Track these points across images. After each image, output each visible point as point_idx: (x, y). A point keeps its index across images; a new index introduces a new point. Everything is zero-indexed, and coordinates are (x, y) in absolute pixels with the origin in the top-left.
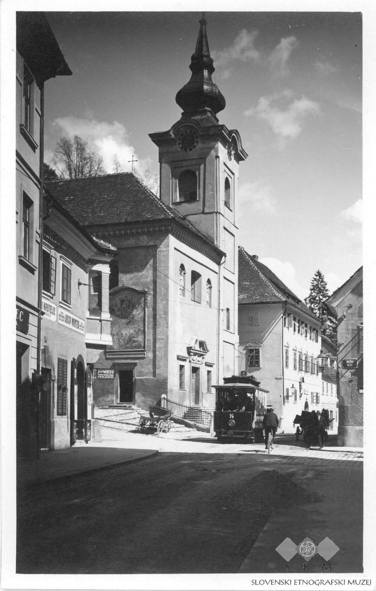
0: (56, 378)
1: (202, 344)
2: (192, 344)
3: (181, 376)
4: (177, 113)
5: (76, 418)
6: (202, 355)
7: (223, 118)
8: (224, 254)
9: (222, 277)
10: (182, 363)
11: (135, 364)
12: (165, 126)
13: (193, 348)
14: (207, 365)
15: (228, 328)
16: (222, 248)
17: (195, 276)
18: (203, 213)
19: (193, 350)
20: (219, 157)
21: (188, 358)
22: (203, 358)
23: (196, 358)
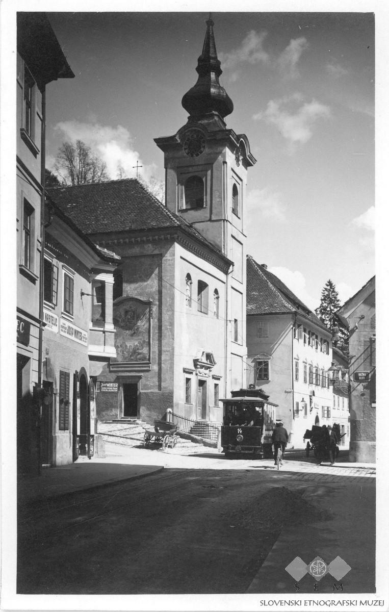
0: (58, 392)
1: (209, 356)
2: (199, 357)
3: (188, 389)
4: (183, 117)
5: (79, 433)
6: (209, 368)
7: (231, 122)
9: (229, 287)
10: (188, 376)
11: (140, 377)
12: (171, 130)
13: (200, 361)
15: (236, 339)
17: (202, 286)
18: (210, 220)
20: (226, 163)
21: (194, 371)
23: (203, 370)
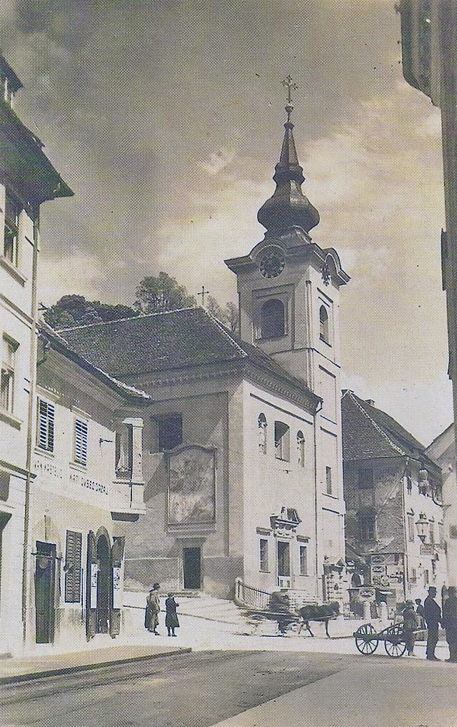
0: (64, 556)
1: (292, 513)
2: (278, 513)
3: (263, 554)
4: (260, 232)
5: (94, 606)
6: (293, 527)
7: (318, 235)
9: (318, 429)
10: (264, 537)
11: (203, 540)
12: (243, 248)
13: (279, 518)
15: (329, 491)
17: (281, 429)
18: (292, 349)
20: (310, 282)
21: (271, 531)
23: (284, 531)
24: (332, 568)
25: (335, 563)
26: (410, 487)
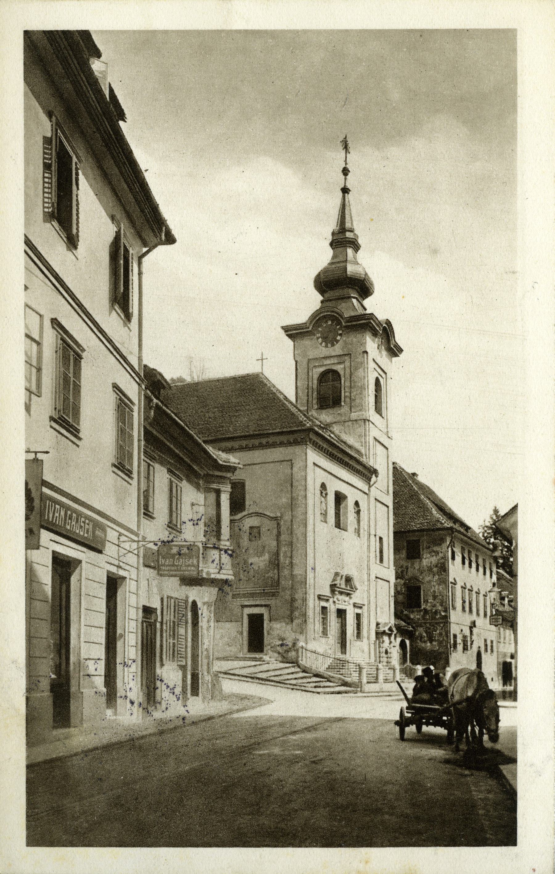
1: (348, 580)
8: (375, 472)
14: (355, 605)
15: (381, 560)
16: (371, 463)
17: (340, 498)
19: (338, 588)
20: (367, 352)
21: (330, 597)
22: (351, 598)
23: (343, 597)
24: (384, 633)
25: (386, 629)
26: (453, 558)
